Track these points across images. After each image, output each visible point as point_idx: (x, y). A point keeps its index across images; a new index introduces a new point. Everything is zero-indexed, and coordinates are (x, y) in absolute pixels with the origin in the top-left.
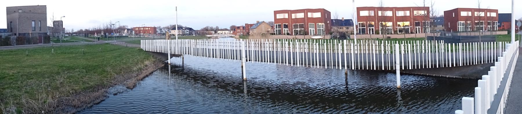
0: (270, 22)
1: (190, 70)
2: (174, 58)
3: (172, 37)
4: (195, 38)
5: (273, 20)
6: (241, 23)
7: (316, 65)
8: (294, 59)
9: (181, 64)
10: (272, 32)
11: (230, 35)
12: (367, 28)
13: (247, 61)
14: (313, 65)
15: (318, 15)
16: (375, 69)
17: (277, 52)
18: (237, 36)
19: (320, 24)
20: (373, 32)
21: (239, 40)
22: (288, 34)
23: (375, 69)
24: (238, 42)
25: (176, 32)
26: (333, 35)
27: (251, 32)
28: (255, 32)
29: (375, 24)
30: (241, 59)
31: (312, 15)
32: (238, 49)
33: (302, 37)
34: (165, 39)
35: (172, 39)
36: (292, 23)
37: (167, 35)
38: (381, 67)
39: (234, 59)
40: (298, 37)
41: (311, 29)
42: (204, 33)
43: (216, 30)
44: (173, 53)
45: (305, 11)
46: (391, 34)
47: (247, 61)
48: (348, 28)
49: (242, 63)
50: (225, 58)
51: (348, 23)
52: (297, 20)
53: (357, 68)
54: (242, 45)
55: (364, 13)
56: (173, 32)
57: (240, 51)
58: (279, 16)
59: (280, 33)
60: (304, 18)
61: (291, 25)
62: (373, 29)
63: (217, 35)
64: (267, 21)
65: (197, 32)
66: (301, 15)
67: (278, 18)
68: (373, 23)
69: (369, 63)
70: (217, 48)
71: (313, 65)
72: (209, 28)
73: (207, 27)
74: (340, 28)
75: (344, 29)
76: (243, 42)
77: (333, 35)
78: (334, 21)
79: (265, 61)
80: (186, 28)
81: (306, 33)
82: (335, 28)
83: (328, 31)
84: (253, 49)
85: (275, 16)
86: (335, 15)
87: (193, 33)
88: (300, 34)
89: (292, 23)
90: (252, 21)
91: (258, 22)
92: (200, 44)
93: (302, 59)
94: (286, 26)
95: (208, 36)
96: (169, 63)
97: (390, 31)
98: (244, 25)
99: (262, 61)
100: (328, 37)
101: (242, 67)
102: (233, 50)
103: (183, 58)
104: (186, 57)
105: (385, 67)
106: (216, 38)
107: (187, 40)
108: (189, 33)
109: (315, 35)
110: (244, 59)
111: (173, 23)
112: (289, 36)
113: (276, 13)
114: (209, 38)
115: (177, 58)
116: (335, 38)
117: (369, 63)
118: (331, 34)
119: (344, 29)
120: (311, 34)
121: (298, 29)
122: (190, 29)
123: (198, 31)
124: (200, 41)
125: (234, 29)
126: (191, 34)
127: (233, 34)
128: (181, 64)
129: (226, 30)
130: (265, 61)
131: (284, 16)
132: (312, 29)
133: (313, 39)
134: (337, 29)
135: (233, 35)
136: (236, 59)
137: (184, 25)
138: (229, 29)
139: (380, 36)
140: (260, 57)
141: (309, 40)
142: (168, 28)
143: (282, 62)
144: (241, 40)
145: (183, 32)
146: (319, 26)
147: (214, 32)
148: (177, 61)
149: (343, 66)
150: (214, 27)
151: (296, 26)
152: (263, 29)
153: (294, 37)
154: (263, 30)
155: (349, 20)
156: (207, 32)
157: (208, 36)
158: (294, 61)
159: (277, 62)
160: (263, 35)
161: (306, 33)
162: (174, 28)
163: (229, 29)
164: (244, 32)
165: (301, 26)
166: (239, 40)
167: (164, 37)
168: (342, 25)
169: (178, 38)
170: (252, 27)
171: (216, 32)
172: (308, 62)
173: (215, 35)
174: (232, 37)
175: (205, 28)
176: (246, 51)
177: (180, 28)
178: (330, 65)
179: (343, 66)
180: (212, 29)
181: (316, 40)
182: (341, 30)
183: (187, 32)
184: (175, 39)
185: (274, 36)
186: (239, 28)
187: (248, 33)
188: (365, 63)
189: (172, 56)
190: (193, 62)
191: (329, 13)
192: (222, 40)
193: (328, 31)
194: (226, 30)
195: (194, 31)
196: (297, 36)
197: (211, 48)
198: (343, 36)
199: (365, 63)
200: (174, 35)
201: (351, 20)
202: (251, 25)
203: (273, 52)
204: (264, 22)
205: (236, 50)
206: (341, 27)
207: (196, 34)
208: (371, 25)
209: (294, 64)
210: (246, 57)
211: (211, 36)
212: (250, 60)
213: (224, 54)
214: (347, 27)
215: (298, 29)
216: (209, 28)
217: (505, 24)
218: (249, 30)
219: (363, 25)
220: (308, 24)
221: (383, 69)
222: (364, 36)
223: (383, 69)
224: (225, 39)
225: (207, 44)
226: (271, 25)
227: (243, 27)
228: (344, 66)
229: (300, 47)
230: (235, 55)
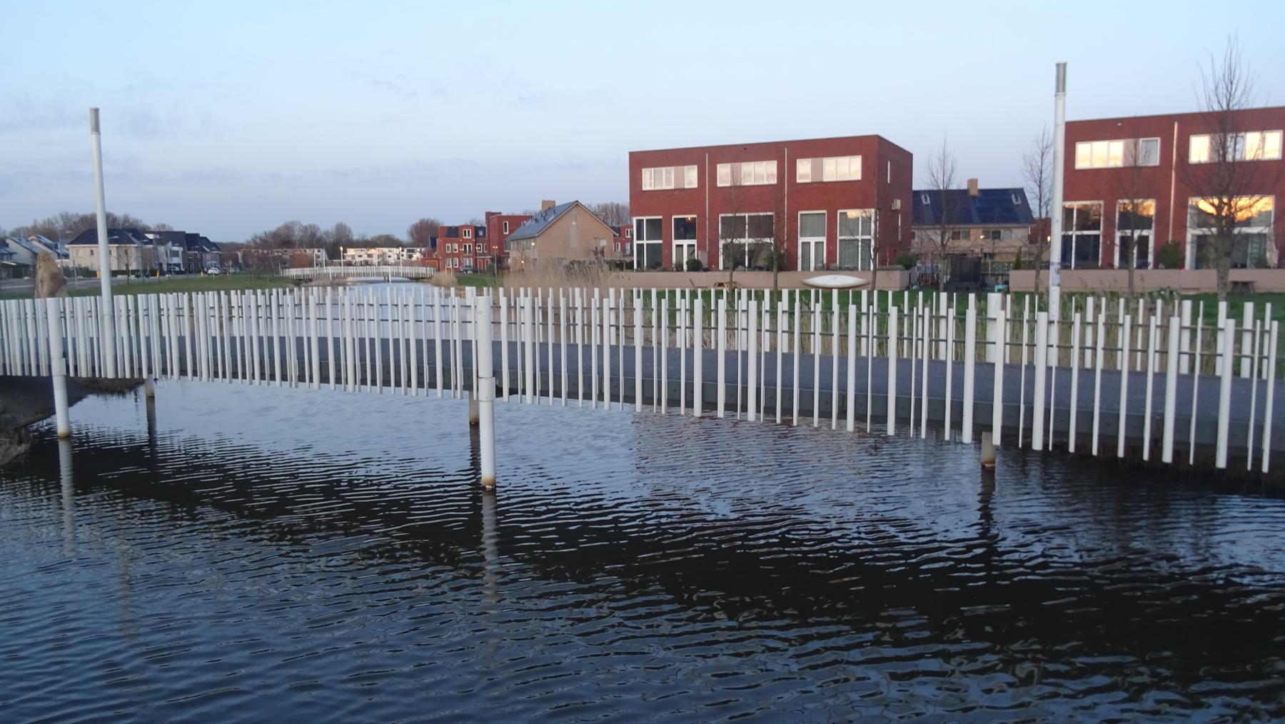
0: (605, 208)
1: (195, 463)
2: (91, 401)
3: (78, 282)
4: (221, 284)
5: (622, 197)
6: (462, 210)
7: (842, 414)
8: (731, 380)
9: (140, 430)
10: (618, 257)
11: (408, 270)
12: (1109, 236)
13: (499, 392)
14: (825, 414)
15: (848, 169)
16: (1167, 457)
17: (647, 350)
18: (447, 276)
19: (853, 213)
20: (1143, 254)
21: (461, 295)
22: (695, 266)
23: (1167, 457)
24: (454, 300)
25: (100, 257)
26: (916, 272)
27: (514, 254)
28: (532, 254)
29: (1162, 210)
30: (468, 386)
31: (818, 170)
32: (455, 335)
33: (763, 280)
34: (31, 294)
35: (73, 293)
36: (715, 210)
37: (42, 273)
38: (1207, 449)
39: (433, 385)
40: (743, 277)
41: (811, 242)
42: (271, 260)
43: (336, 245)
44: (83, 373)
45: (784, 153)
46: (1262, 263)
47: (499, 392)
48: (996, 235)
49: (475, 404)
50: (386, 383)
51: (999, 206)
52: (741, 195)
53: (1061, 445)
54: (474, 316)
55: (1101, 155)
56: (79, 255)
57: (467, 345)
58: (652, 180)
59: (657, 260)
60: (778, 187)
61: (716, 217)
62: (1143, 241)
63: (341, 270)
64: (592, 200)
65: (227, 253)
66: (762, 173)
67: (648, 185)
68: (1150, 207)
69: (1135, 421)
70: (349, 334)
71: (825, 414)
72: (297, 234)
73: (288, 228)
74: (956, 236)
75: (975, 240)
76: (477, 301)
77: (916, 272)
78: (926, 201)
79: (588, 396)
80: (167, 236)
81: (784, 261)
82: (929, 238)
83: (893, 251)
84: (526, 335)
85: (635, 180)
86: (935, 163)
87: (209, 258)
88: (752, 267)
89: (715, 210)
90: (520, 200)
91: (549, 208)
92: (249, 314)
93: (771, 384)
94: (686, 229)
95: (294, 272)
96: (61, 429)
97: (1252, 249)
98: (481, 220)
99: (573, 394)
100: (893, 280)
101: (475, 425)
102: (431, 343)
103: (151, 398)
104: (168, 390)
105: (1236, 454)
106: (337, 282)
107: (169, 300)
108: (187, 260)
109: (828, 268)
110: (485, 387)
111: (82, 201)
112: (700, 278)
113: (639, 161)
114: (298, 282)
115: (115, 401)
116: (930, 285)
117: (1135, 421)
118: (908, 266)
119: (975, 240)
120: (806, 267)
121: (747, 241)
122: (191, 241)
123: (236, 246)
124: (248, 301)
125: (430, 237)
126: (193, 266)
127: (423, 263)
128: (141, 431)
129: (390, 242)
130: (588, 396)
131: (680, 177)
132: (812, 240)
133: (827, 291)
134: (940, 233)
135: (422, 270)
136: (447, 385)
137: (150, 218)
138: (404, 237)
139: (1189, 276)
140: (566, 377)
141: (805, 294)
142: (51, 235)
143: (673, 402)
144: (470, 290)
145: (144, 257)
146: (851, 226)
147: (323, 255)
148: (113, 419)
149: (982, 427)
150: (326, 226)
151: (734, 227)
152: (574, 239)
153: (725, 277)
154: (574, 243)
155: (1005, 192)
156: (288, 254)
157: (294, 272)
158: (731, 392)
159: (647, 400)
160: (576, 271)
161: (784, 261)
162: (85, 233)
163: (404, 237)
164: (480, 250)
165: (761, 227)
166: (461, 295)
167: (22, 284)
168: (968, 220)
169: (116, 290)
170: (519, 233)
171: (334, 254)
172: (794, 401)
173: (330, 270)
174: (417, 279)
175: (275, 235)
176: (496, 346)
177: (123, 232)
178: (903, 417)
179: (982, 427)
180: (313, 239)
181: (843, 291)
182: (962, 245)
183: (172, 255)
184: (97, 291)
185: (626, 274)
186: (453, 232)
187: (500, 260)
188: (1110, 419)
189: (78, 389)
190: (201, 415)
191: (903, 159)
192: (370, 294)
193: (893, 251)
194: (390, 242)
195: (216, 246)
196: (739, 276)
197: (312, 332)
198: (971, 278)
199: (1110, 419)
200: (90, 273)
201: (1020, 192)
202: (516, 221)
203: (630, 350)
204: (577, 204)
205: (445, 343)
206: (962, 227)
207: (222, 262)
208: (1133, 220)
209: (730, 406)
210: (497, 373)
211: (307, 271)
212: (513, 391)
213: (382, 366)
214: (992, 227)
215: (747, 241)
216: (297, 234)
217: (686, 231)
218: (502, 243)
219: (1086, 220)
220: (793, 218)
221: (1221, 462)
222: (1092, 278)
223: (1221, 462)
224: (389, 292)
225: (289, 312)
226: (611, 219)
227: (476, 229)
228: (989, 428)
229: (752, 328)
230: (439, 367)
